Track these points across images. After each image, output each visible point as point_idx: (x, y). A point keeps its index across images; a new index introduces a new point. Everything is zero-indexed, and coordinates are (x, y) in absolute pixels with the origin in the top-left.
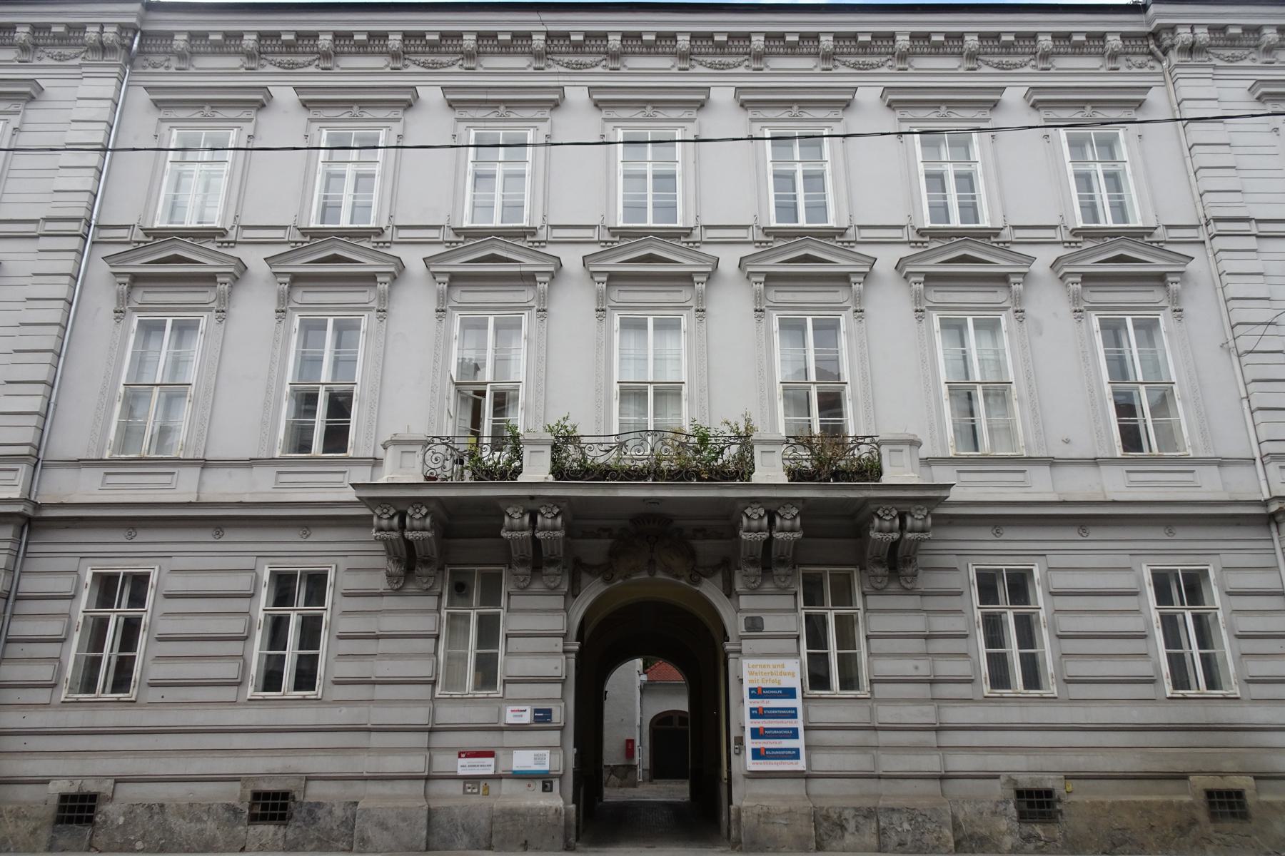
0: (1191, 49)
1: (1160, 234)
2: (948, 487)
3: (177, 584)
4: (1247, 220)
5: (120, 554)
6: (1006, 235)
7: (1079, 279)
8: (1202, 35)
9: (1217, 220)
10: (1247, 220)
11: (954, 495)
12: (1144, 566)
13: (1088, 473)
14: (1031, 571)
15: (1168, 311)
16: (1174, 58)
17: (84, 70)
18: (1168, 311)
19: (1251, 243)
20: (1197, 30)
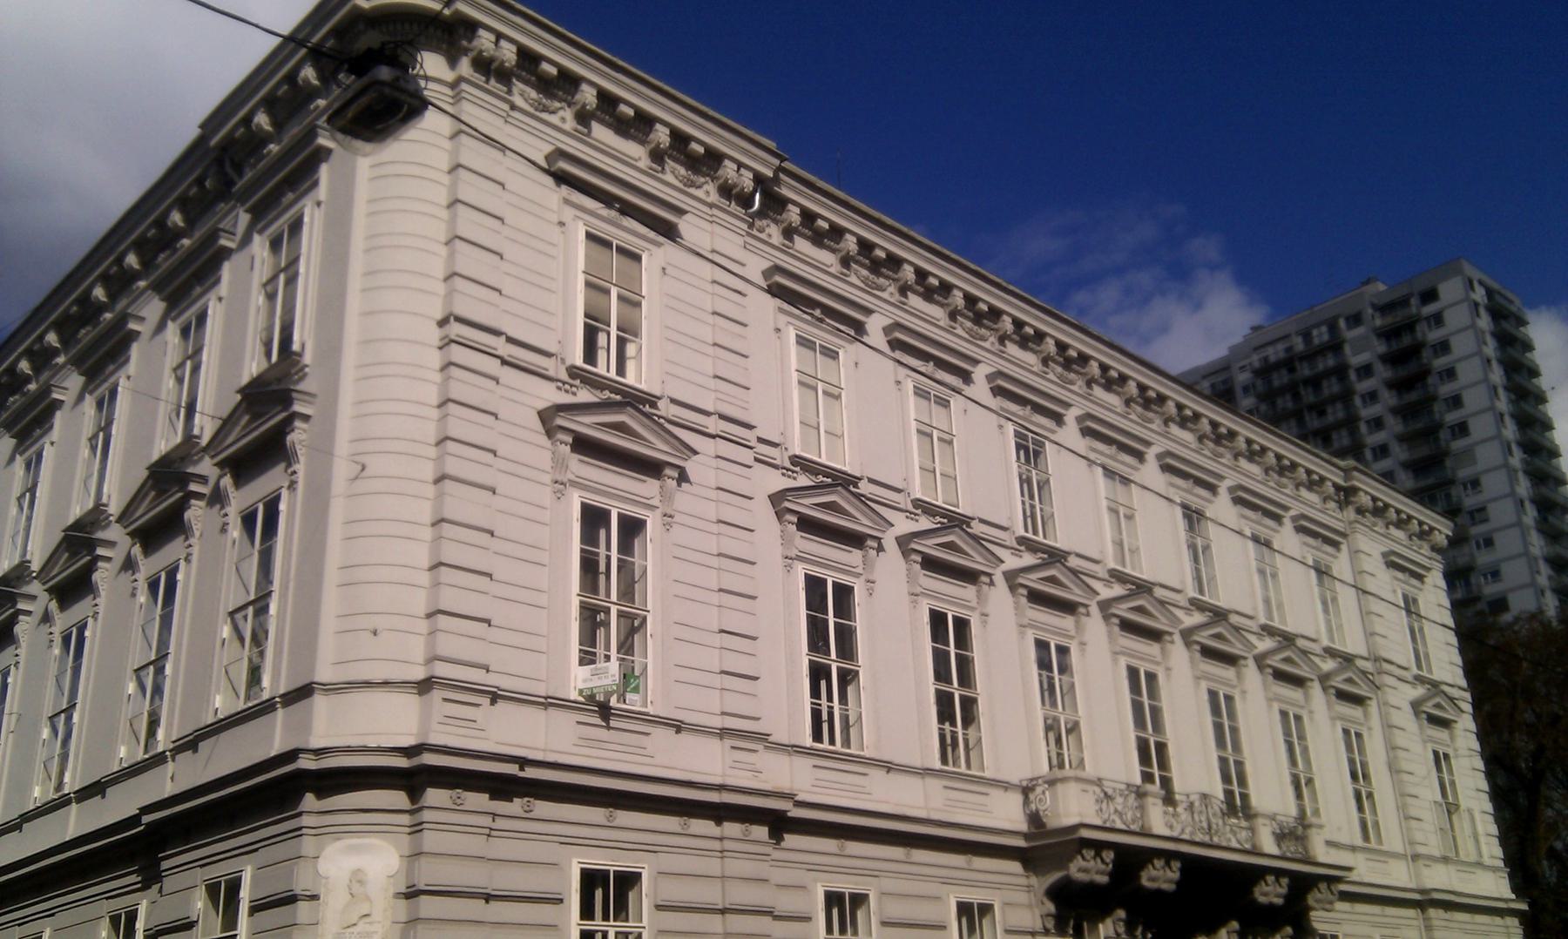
0: (485, 65)
1: (665, 408)
2: (1349, 869)
3: (897, 910)
4: (496, 333)
5: (613, 840)
6: (665, 408)
7: (570, 440)
8: (508, 54)
9: (459, 320)
10: (496, 333)
11: (1353, 876)
12: (575, 861)
13: (914, 782)
14: (640, 874)
15: (658, 512)
16: (465, 67)
17: (715, 212)
18: (658, 512)
19: (492, 366)
20: (503, 43)
